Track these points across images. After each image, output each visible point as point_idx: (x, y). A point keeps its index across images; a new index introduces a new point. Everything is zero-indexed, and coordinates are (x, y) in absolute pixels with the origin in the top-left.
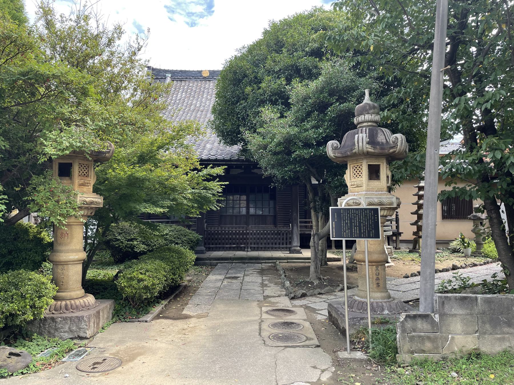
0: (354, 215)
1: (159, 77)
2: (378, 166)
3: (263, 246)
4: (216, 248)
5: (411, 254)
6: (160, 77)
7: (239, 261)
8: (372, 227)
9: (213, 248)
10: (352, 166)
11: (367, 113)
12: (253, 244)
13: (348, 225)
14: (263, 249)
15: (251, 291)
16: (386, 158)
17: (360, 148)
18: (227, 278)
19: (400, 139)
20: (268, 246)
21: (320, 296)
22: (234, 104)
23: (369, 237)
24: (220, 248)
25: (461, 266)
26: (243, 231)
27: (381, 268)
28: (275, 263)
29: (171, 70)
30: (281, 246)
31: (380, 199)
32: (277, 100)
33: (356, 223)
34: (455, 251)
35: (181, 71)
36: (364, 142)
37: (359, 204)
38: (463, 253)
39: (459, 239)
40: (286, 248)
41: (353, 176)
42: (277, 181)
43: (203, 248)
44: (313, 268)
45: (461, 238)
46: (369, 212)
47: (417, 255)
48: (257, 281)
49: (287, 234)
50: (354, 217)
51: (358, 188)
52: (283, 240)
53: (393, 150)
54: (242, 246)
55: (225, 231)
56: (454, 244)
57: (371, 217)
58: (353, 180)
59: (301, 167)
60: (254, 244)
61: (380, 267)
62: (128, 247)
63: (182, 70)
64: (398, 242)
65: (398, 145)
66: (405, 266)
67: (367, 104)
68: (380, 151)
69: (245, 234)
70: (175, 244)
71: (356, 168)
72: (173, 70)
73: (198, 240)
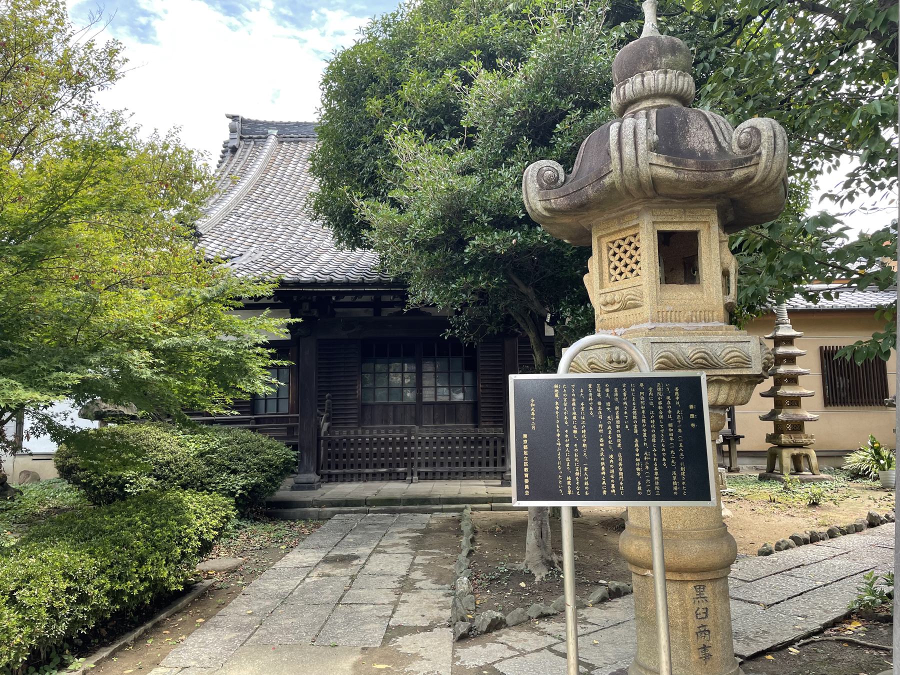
0: (604, 406)
1: (254, 136)
2: (692, 238)
3: (446, 469)
4: (344, 475)
5: (766, 485)
6: (256, 136)
7: (383, 508)
8: (677, 454)
9: (337, 475)
10: (605, 240)
11: (650, 65)
12: (423, 464)
13: (580, 447)
14: (446, 476)
15: (364, 608)
16: (718, 208)
17: (628, 167)
18: (326, 560)
19: (766, 134)
20: (456, 469)
21: (542, 624)
22: (352, 145)
23: (666, 495)
24: (352, 475)
25: (887, 516)
26: (402, 438)
27: (713, 590)
28: (461, 510)
29: (277, 123)
30: (484, 469)
31: (703, 347)
32: (439, 127)
33: (614, 438)
34: (857, 475)
35: (298, 124)
36: (640, 142)
37: (631, 366)
38: (876, 478)
39: (869, 450)
40: (495, 473)
41: (611, 275)
42: (460, 325)
43: (313, 477)
44: (533, 536)
45: (872, 448)
46: (665, 393)
47: (780, 487)
48: (387, 569)
49: (495, 443)
50: (605, 413)
51: (627, 312)
52: (495, 454)
53: (746, 171)
54: (400, 470)
55: (364, 439)
56: (854, 461)
57: (674, 415)
58: (610, 286)
59: (490, 279)
60: (427, 465)
61: (709, 587)
62: (110, 484)
63: (300, 121)
64: (734, 455)
65: (760, 154)
66: (756, 516)
67: (650, 38)
68: (699, 176)
69: (406, 444)
70: (231, 473)
71: (619, 247)
72: (281, 122)
73: (287, 462)
